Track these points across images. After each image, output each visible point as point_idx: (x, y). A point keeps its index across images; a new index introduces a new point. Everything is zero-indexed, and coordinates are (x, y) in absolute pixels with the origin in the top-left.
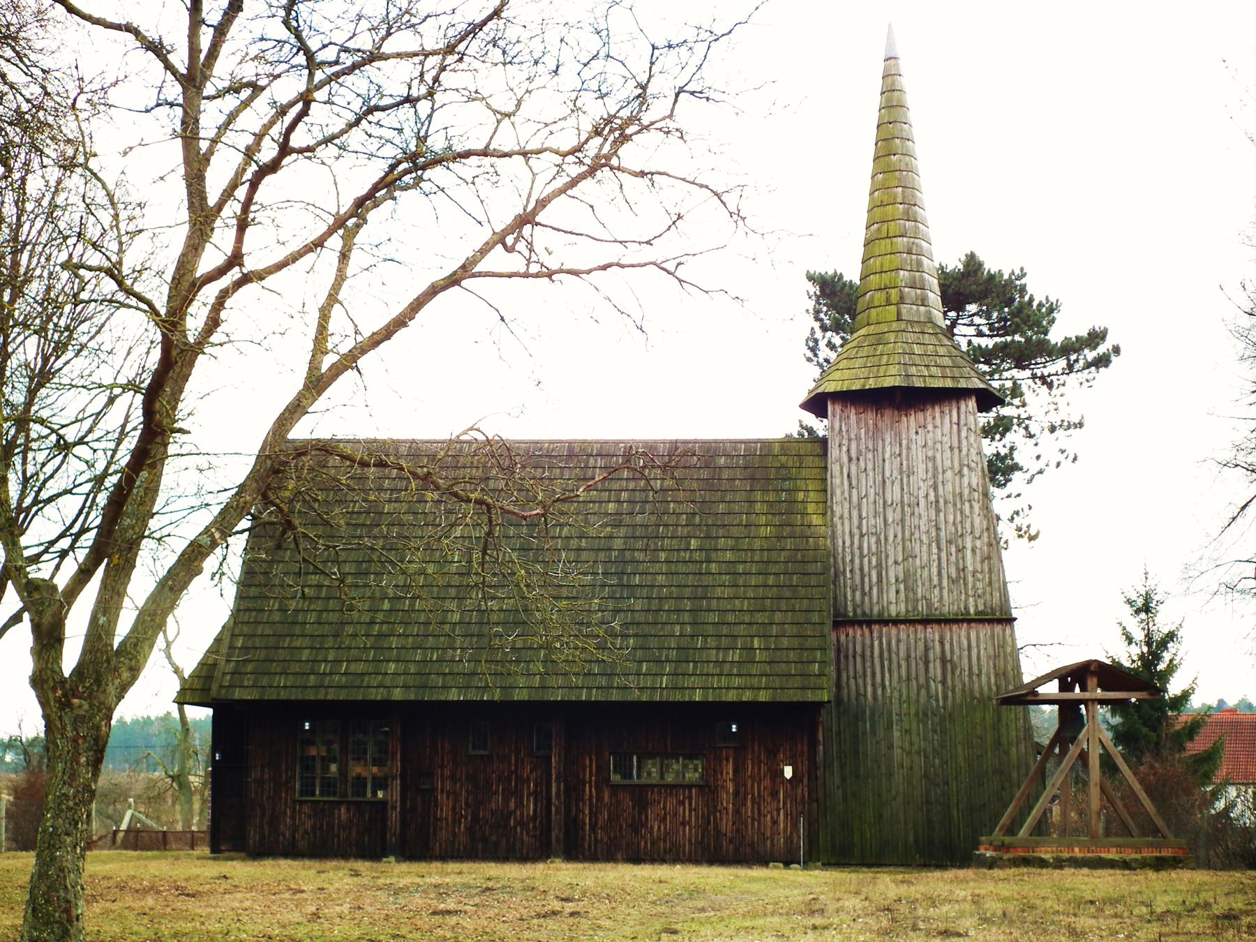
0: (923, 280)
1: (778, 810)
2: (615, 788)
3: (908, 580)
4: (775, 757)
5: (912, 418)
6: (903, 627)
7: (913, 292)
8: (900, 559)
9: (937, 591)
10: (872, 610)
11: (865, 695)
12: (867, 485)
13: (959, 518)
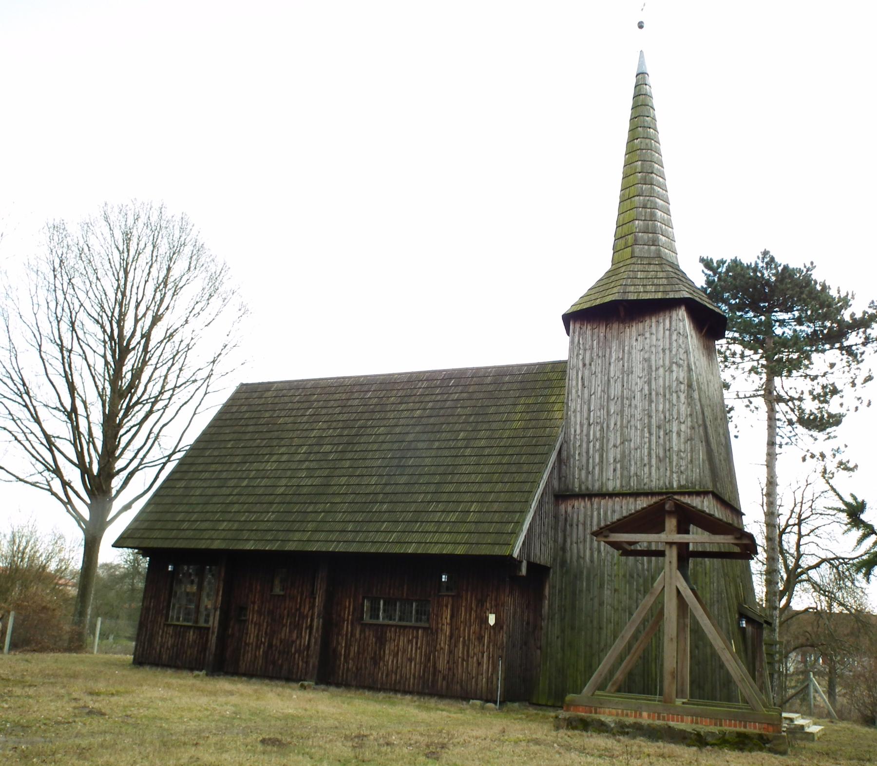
0: (655, 227)
1: (483, 653)
2: (364, 626)
3: (624, 460)
4: (482, 605)
5: (634, 328)
6: (617, 499)
7: (645, 236)
8: (618, 443)
9: (646, 469)
10: (593, 486)
11: (584, 558)
12: (597, 385)
13: (667, 406)
